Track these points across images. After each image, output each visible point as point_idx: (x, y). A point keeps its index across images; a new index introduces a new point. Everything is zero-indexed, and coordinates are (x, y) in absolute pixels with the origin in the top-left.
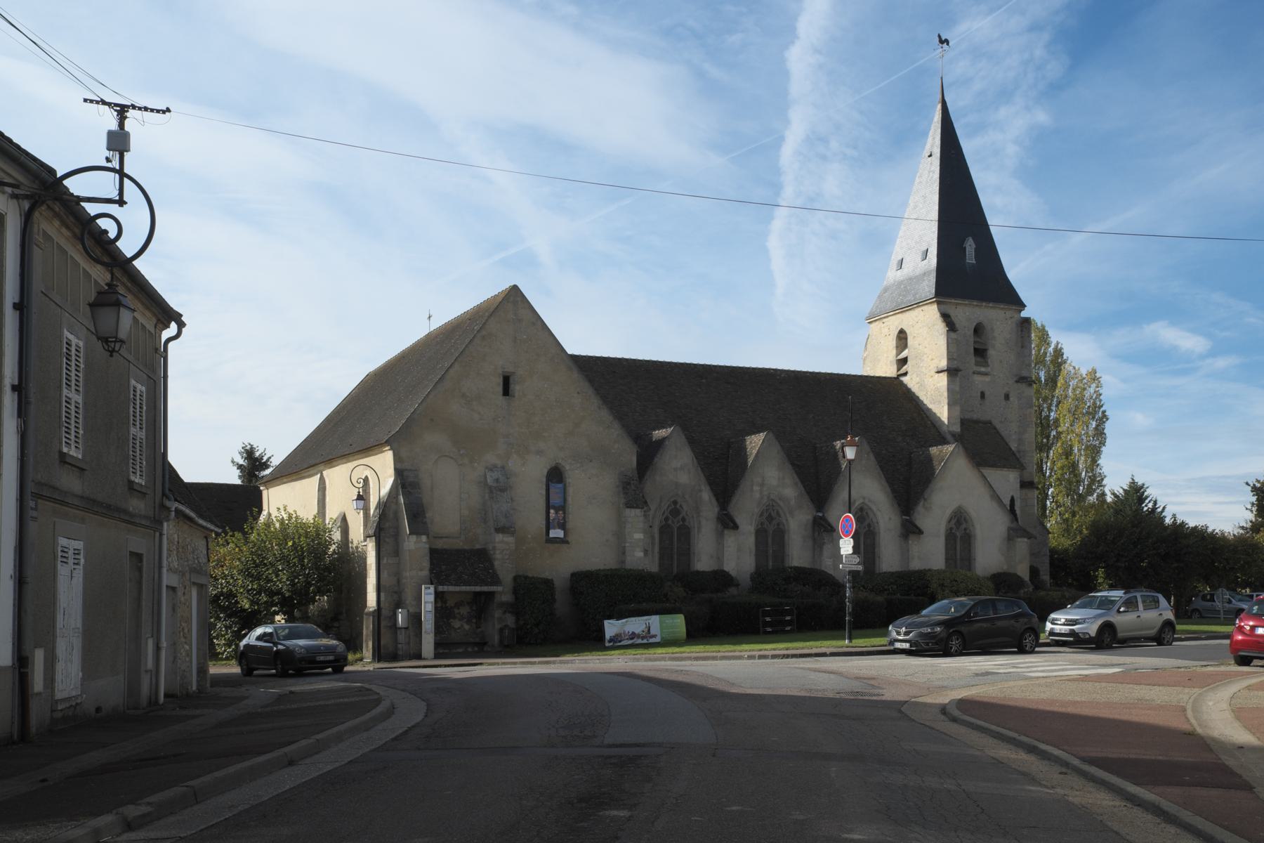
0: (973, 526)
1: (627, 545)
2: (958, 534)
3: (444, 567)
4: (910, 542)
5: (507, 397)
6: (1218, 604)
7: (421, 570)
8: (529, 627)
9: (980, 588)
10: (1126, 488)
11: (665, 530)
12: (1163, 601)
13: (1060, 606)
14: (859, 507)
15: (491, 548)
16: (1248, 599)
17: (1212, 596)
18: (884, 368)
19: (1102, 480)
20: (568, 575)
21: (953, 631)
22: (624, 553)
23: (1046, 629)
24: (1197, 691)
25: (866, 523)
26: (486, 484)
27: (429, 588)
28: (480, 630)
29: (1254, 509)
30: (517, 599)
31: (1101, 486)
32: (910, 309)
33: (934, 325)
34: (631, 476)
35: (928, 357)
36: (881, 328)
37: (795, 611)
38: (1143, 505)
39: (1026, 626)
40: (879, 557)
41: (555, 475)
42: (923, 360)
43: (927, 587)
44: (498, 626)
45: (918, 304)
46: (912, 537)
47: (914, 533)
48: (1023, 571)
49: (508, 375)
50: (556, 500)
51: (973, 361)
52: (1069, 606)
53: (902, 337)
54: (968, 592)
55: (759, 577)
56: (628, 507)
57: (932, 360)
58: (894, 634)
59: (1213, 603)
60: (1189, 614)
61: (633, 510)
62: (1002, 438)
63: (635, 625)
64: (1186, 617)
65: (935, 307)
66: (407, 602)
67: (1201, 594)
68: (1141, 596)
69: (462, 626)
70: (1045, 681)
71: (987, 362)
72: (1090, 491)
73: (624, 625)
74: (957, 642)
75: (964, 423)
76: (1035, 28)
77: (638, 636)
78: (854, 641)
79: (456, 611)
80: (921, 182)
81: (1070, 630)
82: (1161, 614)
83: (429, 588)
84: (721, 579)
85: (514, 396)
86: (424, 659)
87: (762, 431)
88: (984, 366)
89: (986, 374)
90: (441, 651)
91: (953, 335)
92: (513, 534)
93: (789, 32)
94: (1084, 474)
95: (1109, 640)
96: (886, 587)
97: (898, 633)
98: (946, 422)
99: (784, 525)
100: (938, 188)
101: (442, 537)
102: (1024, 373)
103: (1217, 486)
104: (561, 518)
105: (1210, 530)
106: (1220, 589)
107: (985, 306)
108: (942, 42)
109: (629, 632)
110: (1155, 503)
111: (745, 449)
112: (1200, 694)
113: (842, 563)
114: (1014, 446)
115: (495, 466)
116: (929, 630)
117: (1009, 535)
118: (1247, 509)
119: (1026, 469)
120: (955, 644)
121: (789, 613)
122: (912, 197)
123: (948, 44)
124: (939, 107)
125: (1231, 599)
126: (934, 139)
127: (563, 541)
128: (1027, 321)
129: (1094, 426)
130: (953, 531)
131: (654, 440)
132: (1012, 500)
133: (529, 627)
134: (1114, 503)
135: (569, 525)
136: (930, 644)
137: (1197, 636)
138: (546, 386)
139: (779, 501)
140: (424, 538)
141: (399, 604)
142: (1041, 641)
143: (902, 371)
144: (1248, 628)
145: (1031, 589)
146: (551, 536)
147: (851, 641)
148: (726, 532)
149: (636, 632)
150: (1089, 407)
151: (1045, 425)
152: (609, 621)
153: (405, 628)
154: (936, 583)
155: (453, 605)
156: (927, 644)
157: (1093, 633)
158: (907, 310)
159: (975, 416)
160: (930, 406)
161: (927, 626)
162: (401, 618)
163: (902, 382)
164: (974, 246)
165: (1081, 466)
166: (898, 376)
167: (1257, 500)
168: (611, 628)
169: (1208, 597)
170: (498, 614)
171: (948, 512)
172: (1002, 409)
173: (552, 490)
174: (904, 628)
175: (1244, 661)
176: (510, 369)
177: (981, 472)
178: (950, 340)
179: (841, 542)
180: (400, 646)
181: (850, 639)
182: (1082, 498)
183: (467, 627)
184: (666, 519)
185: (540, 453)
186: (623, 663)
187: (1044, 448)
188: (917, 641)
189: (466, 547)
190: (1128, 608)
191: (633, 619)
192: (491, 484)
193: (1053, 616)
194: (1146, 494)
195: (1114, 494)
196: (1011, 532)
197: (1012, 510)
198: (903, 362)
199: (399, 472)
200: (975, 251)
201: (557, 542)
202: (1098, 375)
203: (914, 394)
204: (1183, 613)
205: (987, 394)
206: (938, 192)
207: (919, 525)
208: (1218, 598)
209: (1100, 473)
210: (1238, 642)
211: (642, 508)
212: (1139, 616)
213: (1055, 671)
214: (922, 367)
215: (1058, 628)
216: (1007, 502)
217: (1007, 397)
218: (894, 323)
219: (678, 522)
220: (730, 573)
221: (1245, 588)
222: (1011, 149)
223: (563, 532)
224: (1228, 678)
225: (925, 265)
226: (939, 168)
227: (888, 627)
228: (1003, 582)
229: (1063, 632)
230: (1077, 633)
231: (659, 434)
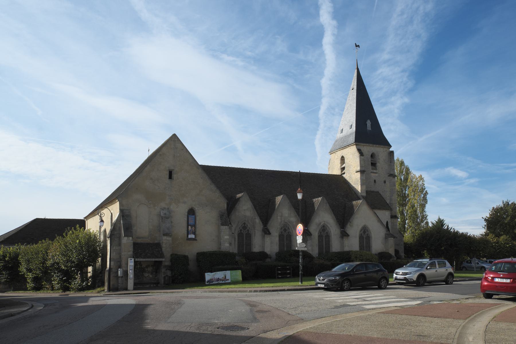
0: (371, 233)
1: (222, 241)
2: (365, 236)
3: (140, 251)
4: (344, 240)
5: (171, 180)
6: (473, 265)
7: (129, 252)
8: (176, 276)
9: (372, 258)
10: (437, 221)
11: (240, 235)
12: (448, 264)
13: (400, 266)
14: (323, 225)
15: (161, 242)
16: (485, 262)
17: (471, 261)
18: (337, 172)
19: (427, 217)
20: (196, 254)
21: (346, 279)
22: (220, 244)
23: (394, 277)
24: (461, 322)
25: (326, 232)
26: (160, 215)
27: (132, 260)
28: (157, 277)
29: (486, 227)
30: (172, 264)
31: (426, 219)
32: (345, 148)
33: (355, 153)
34: (224, 212)
35: (353, 166)
36: (334, 156)
37: (291, 269)
38: (443, 227)
39: (382, 276)
40: (331, 246)
41: (191, 212)
42: (351, 168)
43: (350, 258)
44: (163, 276)
45: (348, 146)
46: (345, 238)
47: (346, 236)
48: (392, 252)
49: (171, 170)
50: (191, 222)
51: (371, 168)
52: (404, 266)
53: (343, 159)
54: (367, 260)
55: (279, 255)
56: (222, 225)
57: (354, 167)
58: (318, 280)
59: (471, 264)
60: (462, 269)
61: (224, 226)
62: (383, 198)
63: (219, 275)
64: (460, 270)
65: (355, 146)
66: (123, 266)
67: (466, 260)
68: (437, 261)
69: (149, 275)
70: (374, 312)
71: (376, 168)
72: (422, 221)
73: (214, 275)
74: (347, 284)
75: (367, 192)
76: (404, 71)
77: (221, 280)
78: (303, 283)
79: (146, 269)
80: (349, 99)
81: (404, 277)
82: (447, 270)
83: (132, 260)
84: (263, 255)
85: (173, 179)
86: (129, 290)
87: (282, 195)
88: (375, 170)
89: (376, 173)
90: (139, 287)
91: (362, 157)
92: (171, 236)
93: (321, 74)
94: (419, 214)
95: (422, 282)
96: (333, 258)
97: (319, 280)
98: (360, 192)
99: (291, 233)
100: (356, 101)
101: (140, 238)
102: (392, 173)
103: (471, 223)
104: (193, 230)
105: (468, 234)
106: (474, 258)
107: (375, 146)
108: (356, 46)
109: (216, 278)
110: (448, 226)
111: (275, 202)
112: (464, 327)
113: (297, 247)
114: (388, 202)
115: (165, 208)
116: (333, 278)
117: (385, 237)
118: (483, 227)
119: (393, 210)
120: (346, 285)
121: (289, 269)
122: (346, 106)
123: (359, 47)
124: (356, 70)
125: (479, 262)
126: (354, 83)
127: (194, 239)
128: (392, 152)
129: (423, 196)
130: (362, 235)
131: (237, 198)
132: (387, 223)
133: (176, 276)
134: (433, 227)
135: (197, 233)
136: (334, 285)
137: (464, 279)
138: (187, 175)
139: (288, 223)
140: (131, 238)
141: (120, 267)
142: (389, 283)
143: (343, 173)
144: (490, 278)
145: (395, 259)
146: (189, 237)
147: (302, 283)
148: (266, 235)
149: (220, 278)
150: (420, 189)
151: (404, 197)
152: (207, 273)
153: (121, 277)
154: (353, 256)
155: (145, 267)
156: (332, 285)
157: (415, 279)
158: (344, 148)
159: (372, 190)
160: (354, 186)
161: (332, 276)
162: (120, 273)
163: (343, 176)
164: (370, 123)
165: (418, 211)
166: (342, 174)
167: (487, 224)
168: (208, 276)
169: (469, 262)
170: (163, 270)
171: (360, 227)
172: (383, 187)
173: (190, 218)
174: (322, 277)
175: (489, 296)
176: (172, 168)
177: (375, 213)
178: (361, 159)
179: (297, 237)
180: (119, 284)
181: (302, 282)
182: (419, 224)
183: (151, 276)
184: (241, 230)
185: (185, 203)
186: (200, 293)
187: (404, 205)
188: (328, 283)
189: (151, 242)
190: (431, 267)
191: (219, 272)
192: (163, 216)
193: (397, 271)
194: (444, 223)
195: (432, 223)
196: (386, 235)
197: (387, 227)
198: (343, 169)
199: (121, 211)
200: (371, 125)
201: (191, 240)
202: (423, 177)
203: (347, 181)
204: (459, 268)
205: (377, 181)
206: (356, 103)
207: (348, 233)
208: (473, 262)
209: (426, 214)
210: (485, 285)
211: (228, 226)
212: (436, 271)
213: (384, 303)
214: (350, 170)
215: (399, 277)
216: (385, 224)
217: (385, 182)
218: (339, 154)
219: (246, 232)
220: (267, 253)
221: (484, 258)
222: (396, 111)
223: (194, 235)
224: (478, 310)
225: (351, 131)
226: (356, 93)
227: (316, 276)
228: (383, 256)
229: (401, 278)
230: (408, 279)
231: (239, 196)
